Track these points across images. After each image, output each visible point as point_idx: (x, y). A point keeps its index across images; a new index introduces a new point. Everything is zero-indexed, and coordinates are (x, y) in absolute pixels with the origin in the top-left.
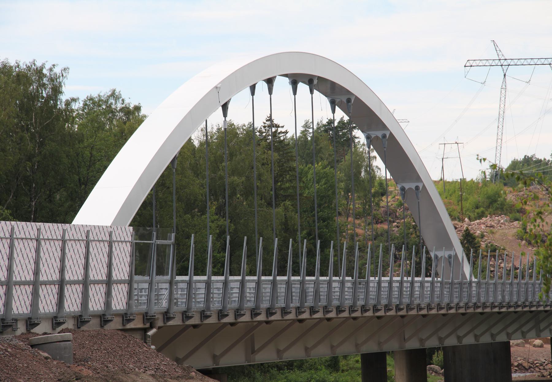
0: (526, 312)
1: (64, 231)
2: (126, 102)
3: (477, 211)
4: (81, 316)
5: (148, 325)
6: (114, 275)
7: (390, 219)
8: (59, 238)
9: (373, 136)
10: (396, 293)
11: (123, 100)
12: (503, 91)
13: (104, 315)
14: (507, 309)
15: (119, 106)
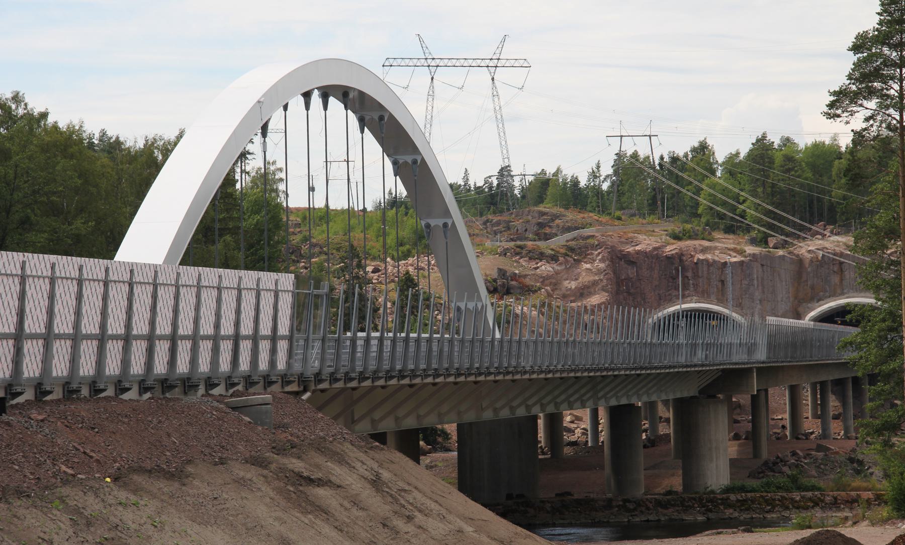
0: (403, 386)
1: (240, 278)
2: (29, 107)
3: (401, 248)
4: (249, 376)
5: (302, 388)
6: (26, 326)
7: (293, 257)
8: (151, 281)
9: (401, 161)
10: (386, 355)
11: (26, 105)
12: (430, 99)
13: (268, 375)
14: (386, 381)
15: (21, 111)
